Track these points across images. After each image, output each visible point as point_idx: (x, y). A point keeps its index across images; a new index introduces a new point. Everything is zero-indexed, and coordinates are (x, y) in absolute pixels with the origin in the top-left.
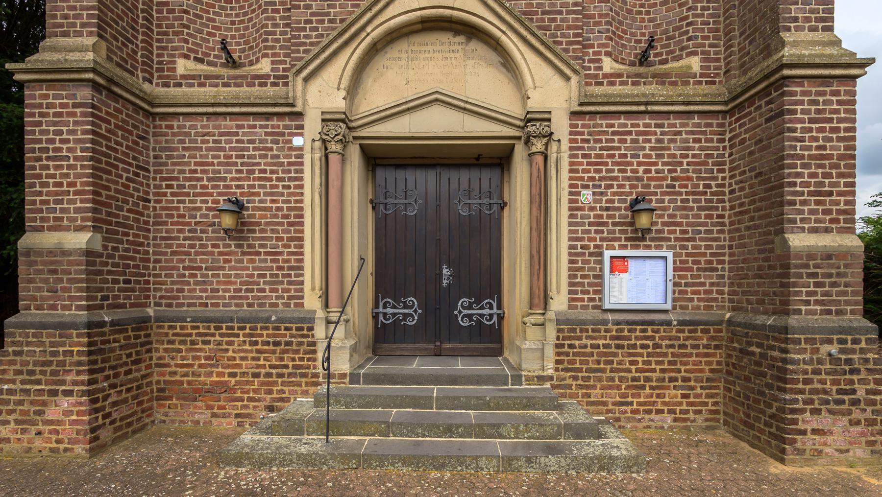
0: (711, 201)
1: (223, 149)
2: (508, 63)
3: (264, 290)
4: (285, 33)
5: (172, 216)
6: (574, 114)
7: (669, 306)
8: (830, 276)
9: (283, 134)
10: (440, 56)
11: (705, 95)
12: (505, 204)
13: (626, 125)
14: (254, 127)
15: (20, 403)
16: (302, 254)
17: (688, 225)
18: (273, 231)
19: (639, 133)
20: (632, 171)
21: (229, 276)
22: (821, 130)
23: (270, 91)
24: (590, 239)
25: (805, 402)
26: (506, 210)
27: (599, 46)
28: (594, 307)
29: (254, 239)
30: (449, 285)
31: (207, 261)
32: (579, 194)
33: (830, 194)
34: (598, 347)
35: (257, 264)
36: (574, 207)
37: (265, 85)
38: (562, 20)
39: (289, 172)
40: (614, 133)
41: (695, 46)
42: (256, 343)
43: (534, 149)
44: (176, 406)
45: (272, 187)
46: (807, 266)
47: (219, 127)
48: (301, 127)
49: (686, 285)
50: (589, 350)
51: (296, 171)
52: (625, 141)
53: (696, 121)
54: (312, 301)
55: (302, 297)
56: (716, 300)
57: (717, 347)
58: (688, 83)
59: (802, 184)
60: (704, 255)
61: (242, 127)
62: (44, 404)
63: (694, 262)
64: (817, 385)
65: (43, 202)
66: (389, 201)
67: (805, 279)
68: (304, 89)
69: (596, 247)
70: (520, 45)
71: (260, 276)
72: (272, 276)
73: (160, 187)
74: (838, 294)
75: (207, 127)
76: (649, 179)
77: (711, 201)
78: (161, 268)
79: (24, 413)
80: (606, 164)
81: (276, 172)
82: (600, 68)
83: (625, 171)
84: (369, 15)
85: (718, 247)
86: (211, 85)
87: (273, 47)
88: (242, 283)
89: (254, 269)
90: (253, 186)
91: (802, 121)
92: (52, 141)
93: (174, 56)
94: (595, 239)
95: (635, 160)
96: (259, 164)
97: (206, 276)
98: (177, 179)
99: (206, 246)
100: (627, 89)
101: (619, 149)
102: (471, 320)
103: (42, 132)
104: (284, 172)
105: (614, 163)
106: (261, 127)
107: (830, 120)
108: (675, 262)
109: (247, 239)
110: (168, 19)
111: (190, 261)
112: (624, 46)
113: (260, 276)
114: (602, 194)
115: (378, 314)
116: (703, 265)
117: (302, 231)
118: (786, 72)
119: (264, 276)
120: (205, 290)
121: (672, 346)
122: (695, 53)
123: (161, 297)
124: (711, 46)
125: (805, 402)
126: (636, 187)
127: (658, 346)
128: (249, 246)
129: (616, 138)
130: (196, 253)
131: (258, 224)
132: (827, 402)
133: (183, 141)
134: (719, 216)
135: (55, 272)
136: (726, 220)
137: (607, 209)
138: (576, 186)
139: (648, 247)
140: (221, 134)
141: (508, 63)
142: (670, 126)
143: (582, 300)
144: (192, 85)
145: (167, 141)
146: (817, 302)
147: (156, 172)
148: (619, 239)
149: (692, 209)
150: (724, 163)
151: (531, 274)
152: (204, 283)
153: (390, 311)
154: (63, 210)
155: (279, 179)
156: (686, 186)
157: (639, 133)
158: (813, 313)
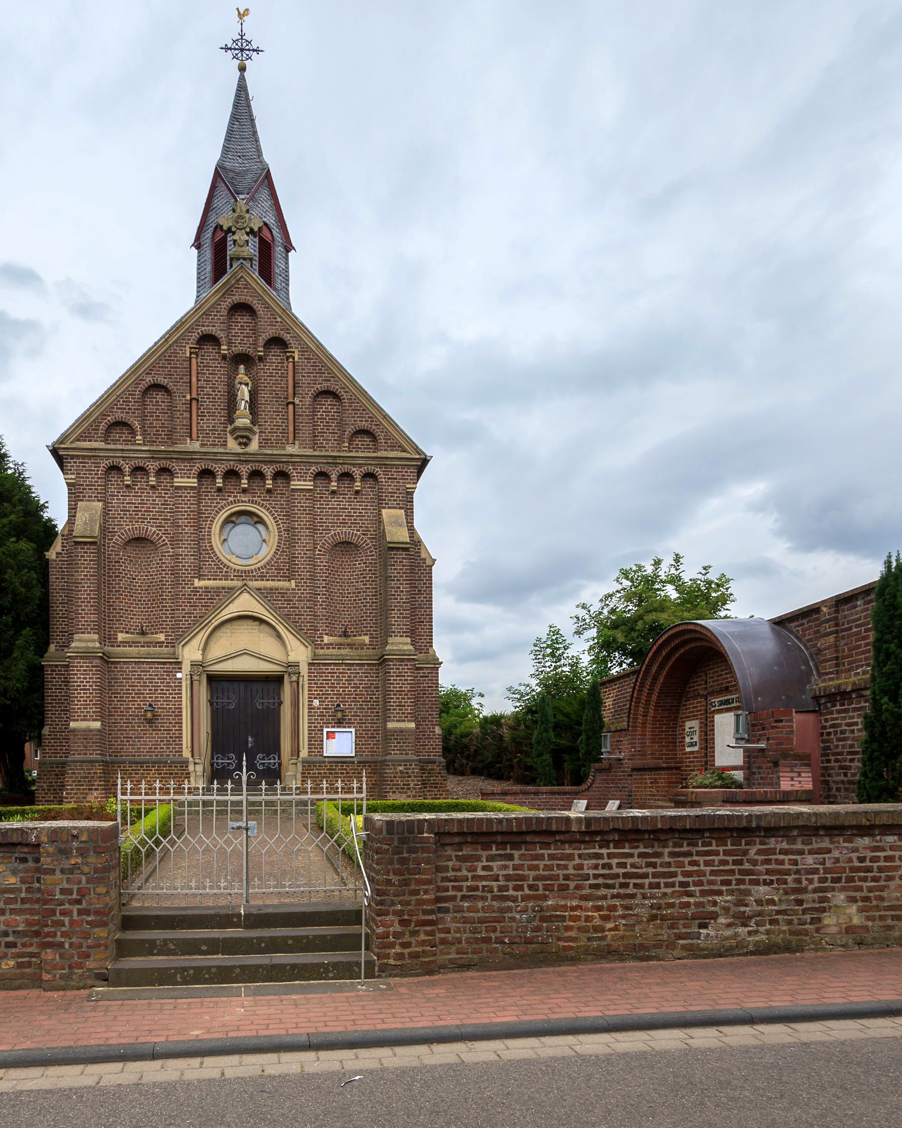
0: (373, 705)
3: (163, 748)
5: (117, 712)
6: (310, 664)
7: (353, 755)
8: (402, 739)
9: (172, 672)
10: (247, 631)
11: (370, 656)
12: (282, 702)
13: (334, 669)
14: (158, 668)
15: (76, 794)
16: (181, 730)
17: (363, 716)
18: (167, 719)
19: (340, 673)
20: (337, 691)
22: (401, 680)
23: (165, 650)
24: (318, 723)
25: (390, 789)
26: (282, 706)
27: (322, 630)
28: (320, 755)
29: (158, 723)
30: (252, 747)
31: (135, 734)
32: (312, 701)
33: (405, 706)
34: (321, 773)
36: (311, 707)
37: (162, 647)
39: (175, 690)
40: (328, 673)
42: (161, 774)
45: (167, 697)
46: (394, 735)
47: (140, 668)
48: (181, 668)
49: (362, 744)
50: (317, 775)
51: (178, 690)
52: (334, 677)
54: (186, 754)
55: (182, 752)
56: (376, 752)
57: (374, 773)
58: (363, 648)
59: (394, 702)
60: (370, 730)
61: (152, 668)
62: (87, 794)
63: (366, 734)
64: (395, 782)
66: (219, 701)
68: (182, 650)
69: (321, 727)
70: (285, 630)
71: (161, 741)
73: (111, 697)
74: (406, 746)
75: (134, 668)
76: (345, 694)
77: (373, 705)
78: (112, 738)
79: (79, 798)
80: (325, 687)
81: (169, 690)
82: (323, 641)
84: (213, 615)
85: (376, 727)
86: (135, 646)
87: (166, 628)
88: (152, 745)
89: (158, 738)
90: (158, 697)
91: (393, 676)
93: (116, 632)
94: (320, 723)
96: (160, 686)
98: (120, 694)
99: (134, 727)
100: (335, 652)
101: (331, 680)
102: (264, 766)
104: (172, 690)
105: (328, 687)
106: (161, 668)
107: (404, 676)
108: (356, 734)
109: (155, 723)
110: (113, 613)
113: (161, 741)
114: (323, 702)
115: (213, 763)
117: (182, 719)
118: (386, 657)
119: (163, 741)
120: (134, 748)
121: (355, 773)
122: (366, 634)
124: (374, 631)
125: (390, 789)
126: (339, 698)
127: (347, 773)
128: (156, 727)
130: (130, 730)
131: (160, 716)
132: (398, 789)
134: (377, 712)
135: (86, 739)
136: (380, 714)
137: (326, 709)
138: (311, 698)
139: (345, 727)
142: (354, 670)
143: (315, 752)
144: (126, 646)
145: (114, 675)
146: (398, 750)
147: (109, 690)
148: (331, 723)
149: (364, 709)
153: (220, 761)
158: (396, 754)
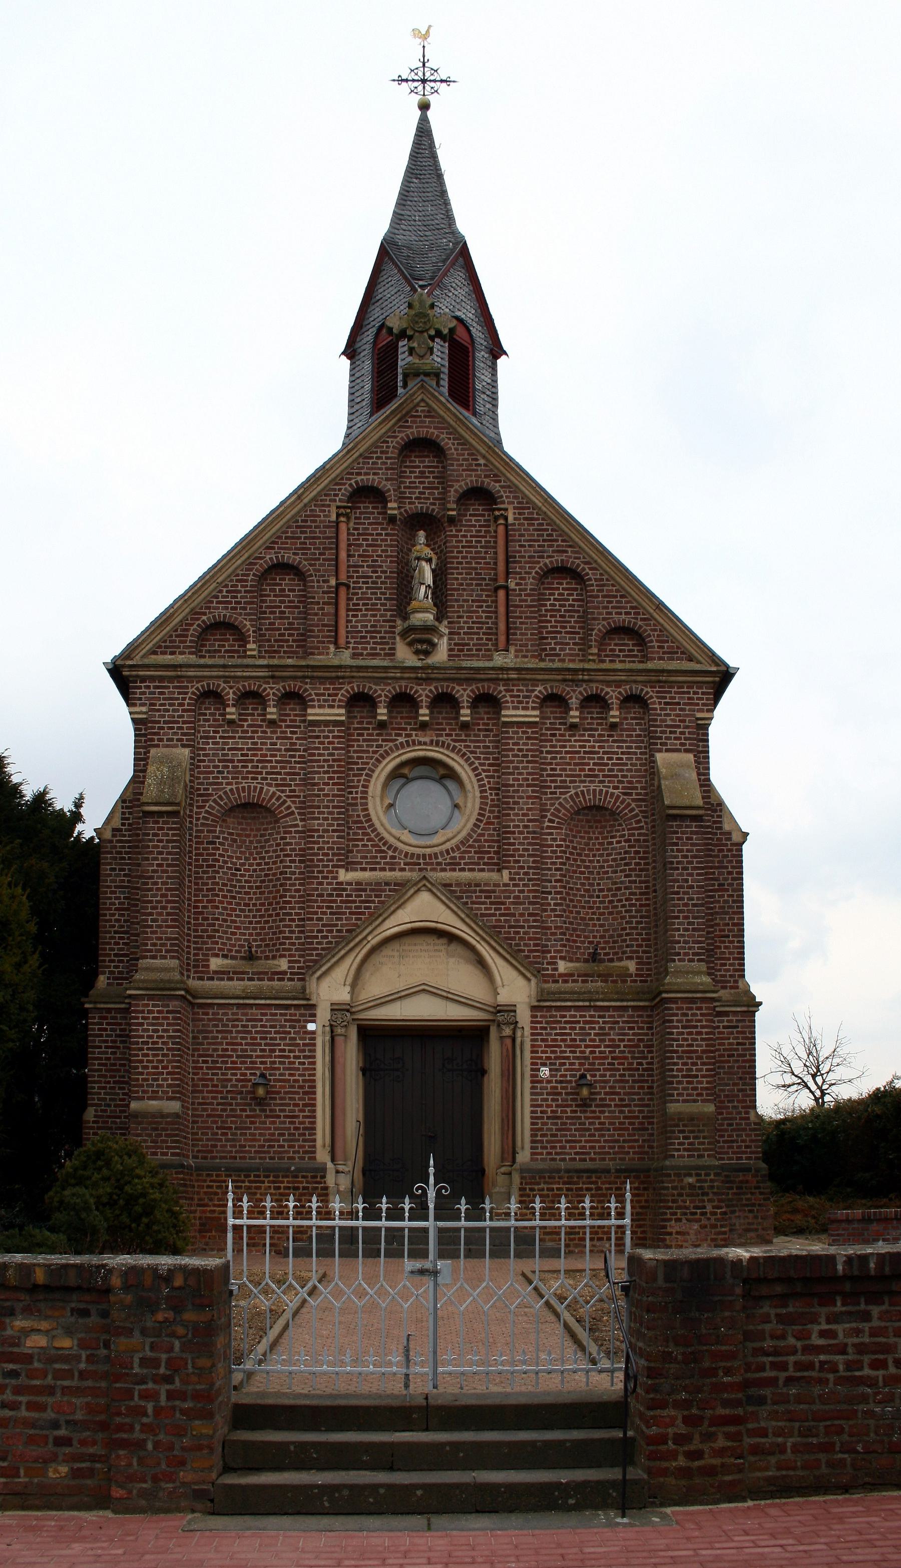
0: (643, 1075)
1: (250, 1032)
2: (481, 963)
3: (283, 1146)
4: (300, 938)
5: (207, 1086)
6: (534, 1008)
8: (693, 1132)
9: (299, 1021)
13: (575, 1016)
14: (276, 1014)
16: (315, 1117)
18: (290, 1099)
19: (585, 1022)
20: (581, 1052)
21: (255, 1135)
24: (548, 1106)
27: (555, 951)
29: (275, 1105)
32: (538, 1070)
33: (697, 1076)
35: (278, 1125)
36: (535, 1080)
38: (524, 933)
39: (304, 1051)
40: (566, 1022)
41: (631, 952)
42: (279, 1188)
43: (504, 1034)
44: (215, 1237)
45: (290, 1063)
46: (678, 1126)
47: (246, 1014)
48: (314, 1015)
53: (630, 1013)
54: (322, 1156)
55: (314, 1152)
57: (645, 1189)
60: (638, 1117)
61: (266, 1014)
64: (680, 1203)
65: (144, 1080)
67: (677, 1134)
70: (491, 952)
71: (280, 1135)
72: (289, 1134)
73: (198, 1062)
75: (237, 1014)
76: (594, 1058)
80: (560, 1046)
82: (556, 969)
83: (575, 1052)
86: (238, 979)
88: (265, 1141)
89: (275, 1129)
90: (274, 1063)
91: (677, 1027)
92: (151, 1037)
93: (207, 955)
95: (583, 1044)
96: (279, 1045)
97: (236, 1134)
98: (212, 1056)
101: (570, 1034)
103: (144, 1030)
104: (300, 1051)
106: (281, 1014)
107: (696, 1027)
111: (223, 1122)
112: (578, 948)
113: (280, 1135)
114: (556, 1070)
116: (636, 1126)
117: (315, 1099)
118: (665, 995)
119: (283, 1135)
120: (235, 1146)
123: (198, 1151)
124: (644, 952)
125: (672, 1214)
128: (271, 1111)
129: (568, 1026)
130: (228, 1116)
133: (217, 1026)
135: (156, 1129)
137: (561, 1082)
138: (536, 1064)
140: (248, 1020)
141: (481, 963)
143: (542, 1154)
144: (222, 979)
146: (685, 1150)
148: (571, 1106)
149: (628, 1081)
150: (652, 1046)
151: (502, 1134)
152: (233, 1140)
154: (159, 1086)
155: (295, 1057)
156: (623, 1064)
157: (585, 1022)
